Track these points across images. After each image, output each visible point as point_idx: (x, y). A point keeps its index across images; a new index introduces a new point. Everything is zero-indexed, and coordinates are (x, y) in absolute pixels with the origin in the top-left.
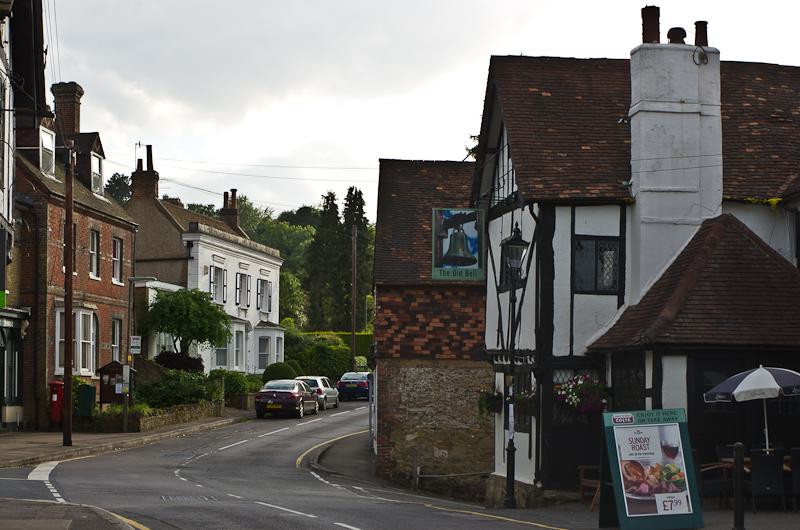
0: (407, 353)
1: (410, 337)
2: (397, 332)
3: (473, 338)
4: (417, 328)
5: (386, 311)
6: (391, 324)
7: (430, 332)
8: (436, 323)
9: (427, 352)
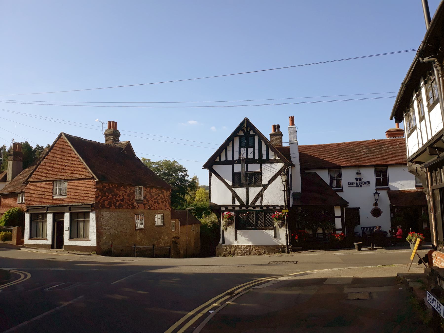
0: (103, 207)
1: (104, 201)
2: (101, 199)
3: (118, 201)
4: (106, 198)
5: (98, 191)
6: (99, 196)
7: (109, 199)
8: (110, 196)
9: (108, 206)
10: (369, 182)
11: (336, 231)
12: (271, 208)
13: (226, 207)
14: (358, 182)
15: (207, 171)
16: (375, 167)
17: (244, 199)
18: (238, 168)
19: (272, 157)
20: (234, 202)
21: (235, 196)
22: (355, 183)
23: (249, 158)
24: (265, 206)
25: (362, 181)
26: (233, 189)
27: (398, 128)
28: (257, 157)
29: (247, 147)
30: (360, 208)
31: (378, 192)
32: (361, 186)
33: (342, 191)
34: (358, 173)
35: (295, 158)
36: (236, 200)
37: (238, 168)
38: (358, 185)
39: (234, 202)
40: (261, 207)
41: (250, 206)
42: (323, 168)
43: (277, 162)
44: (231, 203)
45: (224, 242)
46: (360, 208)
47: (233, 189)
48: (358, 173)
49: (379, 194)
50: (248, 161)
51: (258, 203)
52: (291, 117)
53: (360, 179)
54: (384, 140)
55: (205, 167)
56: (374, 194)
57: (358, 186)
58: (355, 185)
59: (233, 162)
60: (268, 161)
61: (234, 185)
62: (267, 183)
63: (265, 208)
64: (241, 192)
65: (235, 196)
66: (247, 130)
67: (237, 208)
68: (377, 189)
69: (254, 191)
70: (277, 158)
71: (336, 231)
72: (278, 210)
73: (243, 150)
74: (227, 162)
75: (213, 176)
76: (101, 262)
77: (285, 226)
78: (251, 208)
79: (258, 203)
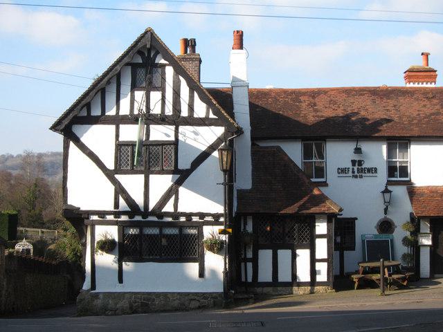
10: (376, 169)
11: (269, 252)
12: (195, 219)
13: (102, 214)
14: (356, 168)
15: (60, 138)
16: (388, 140)
17: (139, 199)
18: (131, 133)
19: (201, 110)
20: (117, 205)
21: (120, 190)
22: (351, 170)
23: (151, 112)
24: (183, 214)
26: (117, 176)
27: (428, 65)
28: (169, 111)
29: (150, 88)
30: (356, 219)
31: (390, 188)
32: (361, 177)
33: (325, 184)
34: (358, 151)
35: (243, 117)
38: (356, 173)
40: (176, 215)
41: (153, 213)
42: (292, 138)
44: (111, 208)
45: (93, 286)
46: (356, 219)
47: (117, 176)
48: (358, 151)
49: (390, 192)
50: (150, 119)
51: (169, 208)
52: (238, 32)
53: (360, 163)
54: (402, 87)
55: (55, 128)
56: (383, 192)
57: (356, 177)
58: (350, 174)
59: (118, 121)
60: (192, 121)
61: (118, 170)
62: (188, 166)
63: (183, 219)
64: (133, 184)
65: (120, 190)
68: (389, 183)
69: (161, 183)
70: (212, 116)
71: (269, 252)
72: (208, 223)
75: (72, 144)
77: (224, 251)
78: (155, 219)
79: (169, 208)
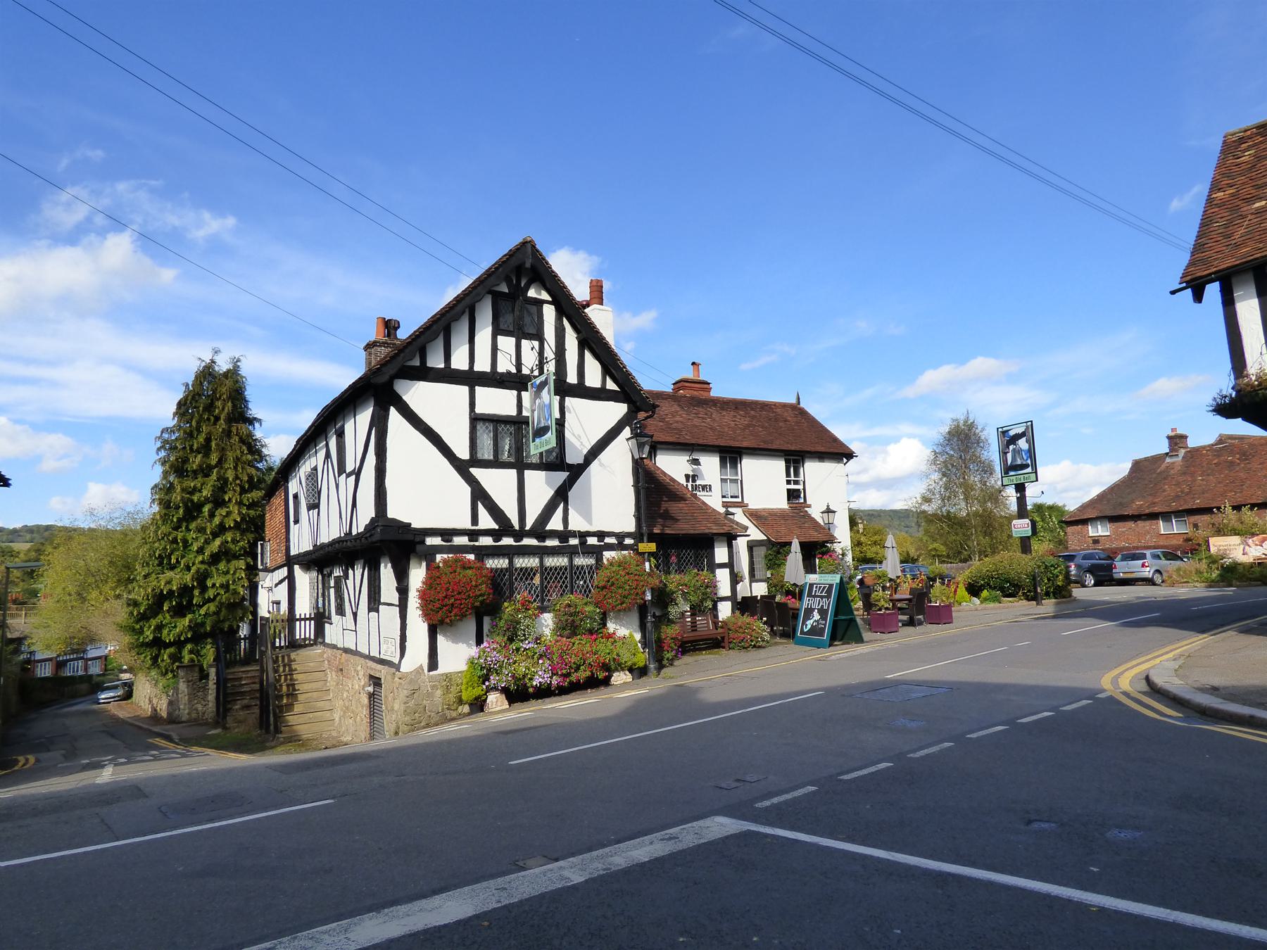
13: (447, 534)
18: (497, 401)
20: (475, 519)
21: (480, 495)
24: (574, 534)
25: (698, 483)
36: (482, 510)
37: (497, 401)
39: (475, 519)
43: (599, 394)
48: (696, 462)
51: (555, 524)
59: (471, 379)
64: (499, 483)
65: (480, 495)
66: (519, 282)
67: (486, 541)
73: (507, 344)
74: (449, 376)
76: (765, 693)
